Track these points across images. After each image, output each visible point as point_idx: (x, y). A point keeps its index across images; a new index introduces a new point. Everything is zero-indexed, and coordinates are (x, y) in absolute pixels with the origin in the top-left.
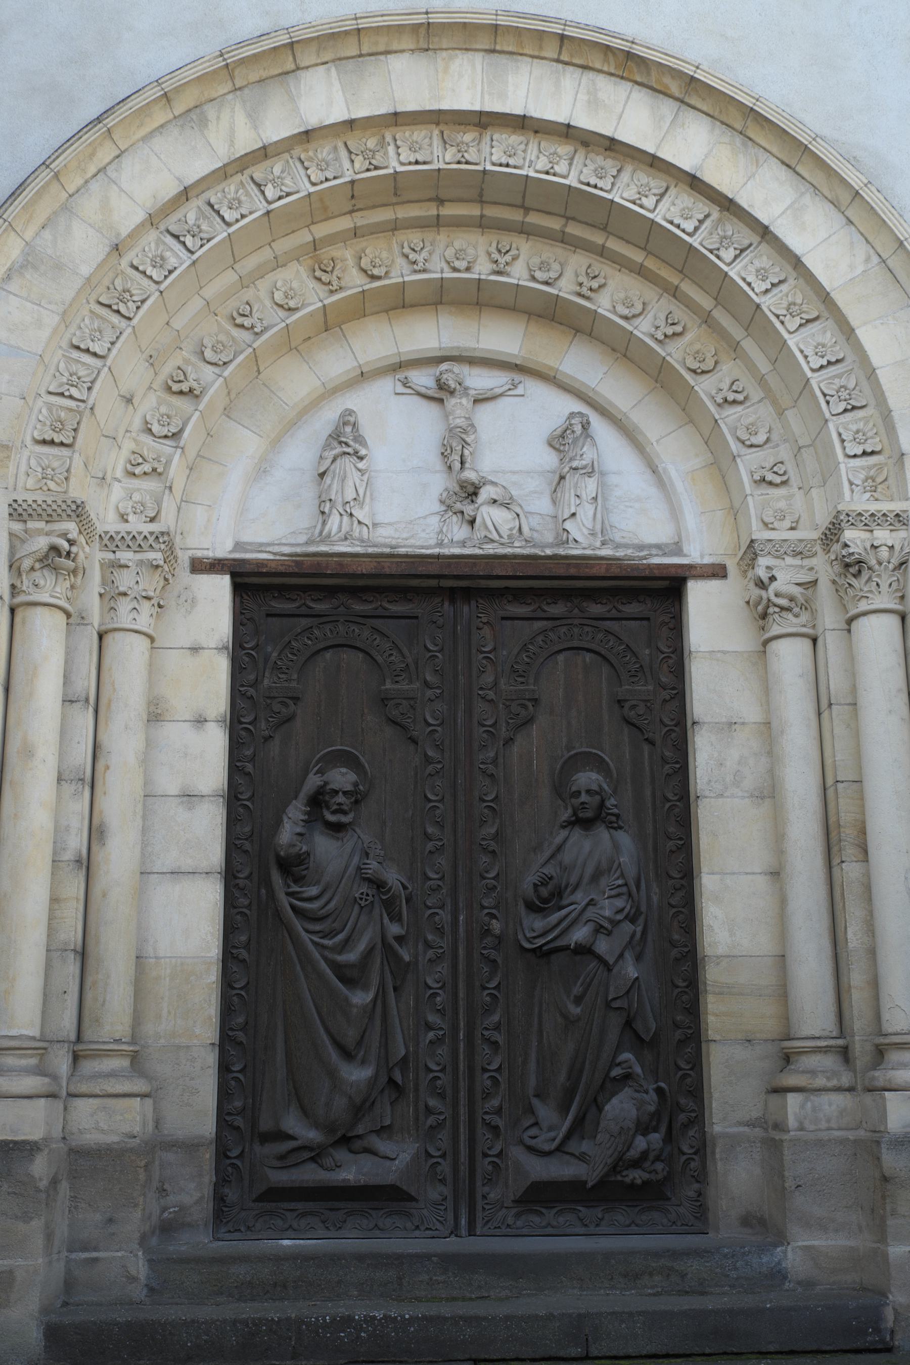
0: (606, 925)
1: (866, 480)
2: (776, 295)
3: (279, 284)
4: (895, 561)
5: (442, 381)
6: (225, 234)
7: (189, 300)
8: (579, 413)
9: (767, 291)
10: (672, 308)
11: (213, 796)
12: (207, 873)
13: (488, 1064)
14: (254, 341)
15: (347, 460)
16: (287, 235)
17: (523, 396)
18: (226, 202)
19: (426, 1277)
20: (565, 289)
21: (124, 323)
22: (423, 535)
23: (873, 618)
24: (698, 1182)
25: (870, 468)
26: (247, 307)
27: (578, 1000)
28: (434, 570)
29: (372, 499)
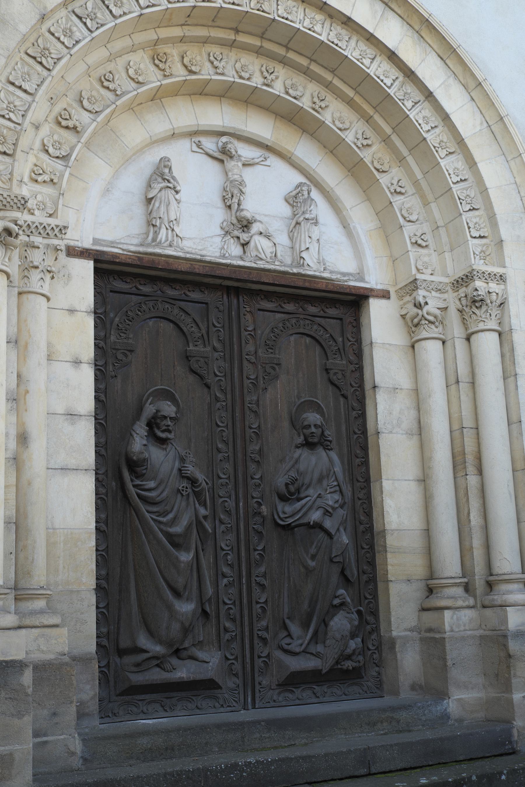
0: (330, 510)
1: (480, 253)
2: (433, 134)
4: (499, 302)
5: (227, 148)
9: (429, 131)
10: (365, 128)
11: (88, 416)
12: (86, 470)
13: (259, 599)
17: (269, 166)
19: (258, 735)
21: (45, 73)
22: (211, 249)
23: (487, 333)
24: (377, 666)
25: (484, 245)
26: (111, 75)
27: (313, 557)
28: (225, 273)
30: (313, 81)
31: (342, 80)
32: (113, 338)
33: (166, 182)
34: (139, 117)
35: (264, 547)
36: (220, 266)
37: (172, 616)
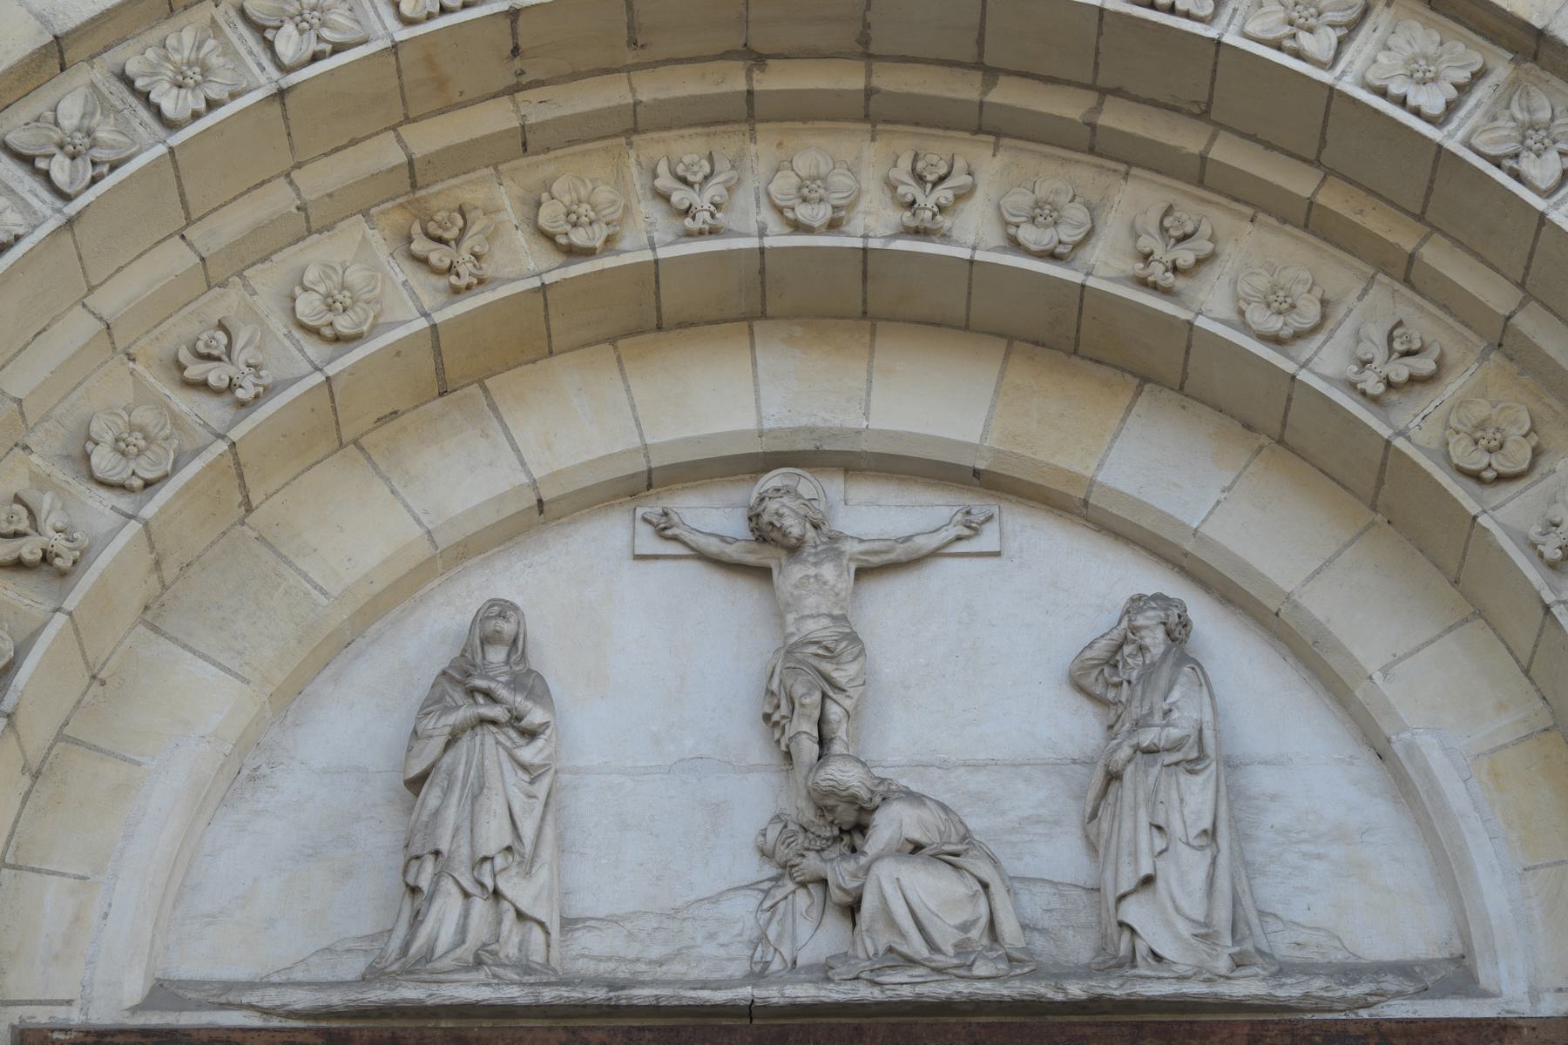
3: (311, 276)
5: (766, 518)
6: (161, 149)
7: (55, 319)
8: (1158, 597)
10: (1404, 311)
14: (234, 424)
15: (490, 741)
16: (337, 150)
17: (997, 554)
18: (168, 71)
20: (1105, 269)
22: (710, 949)
29: (561, 848)
30: (1134, 171)
31: (1253, 138)
33: (481, 699)
34: (382, 467)
36: (714, 1021)
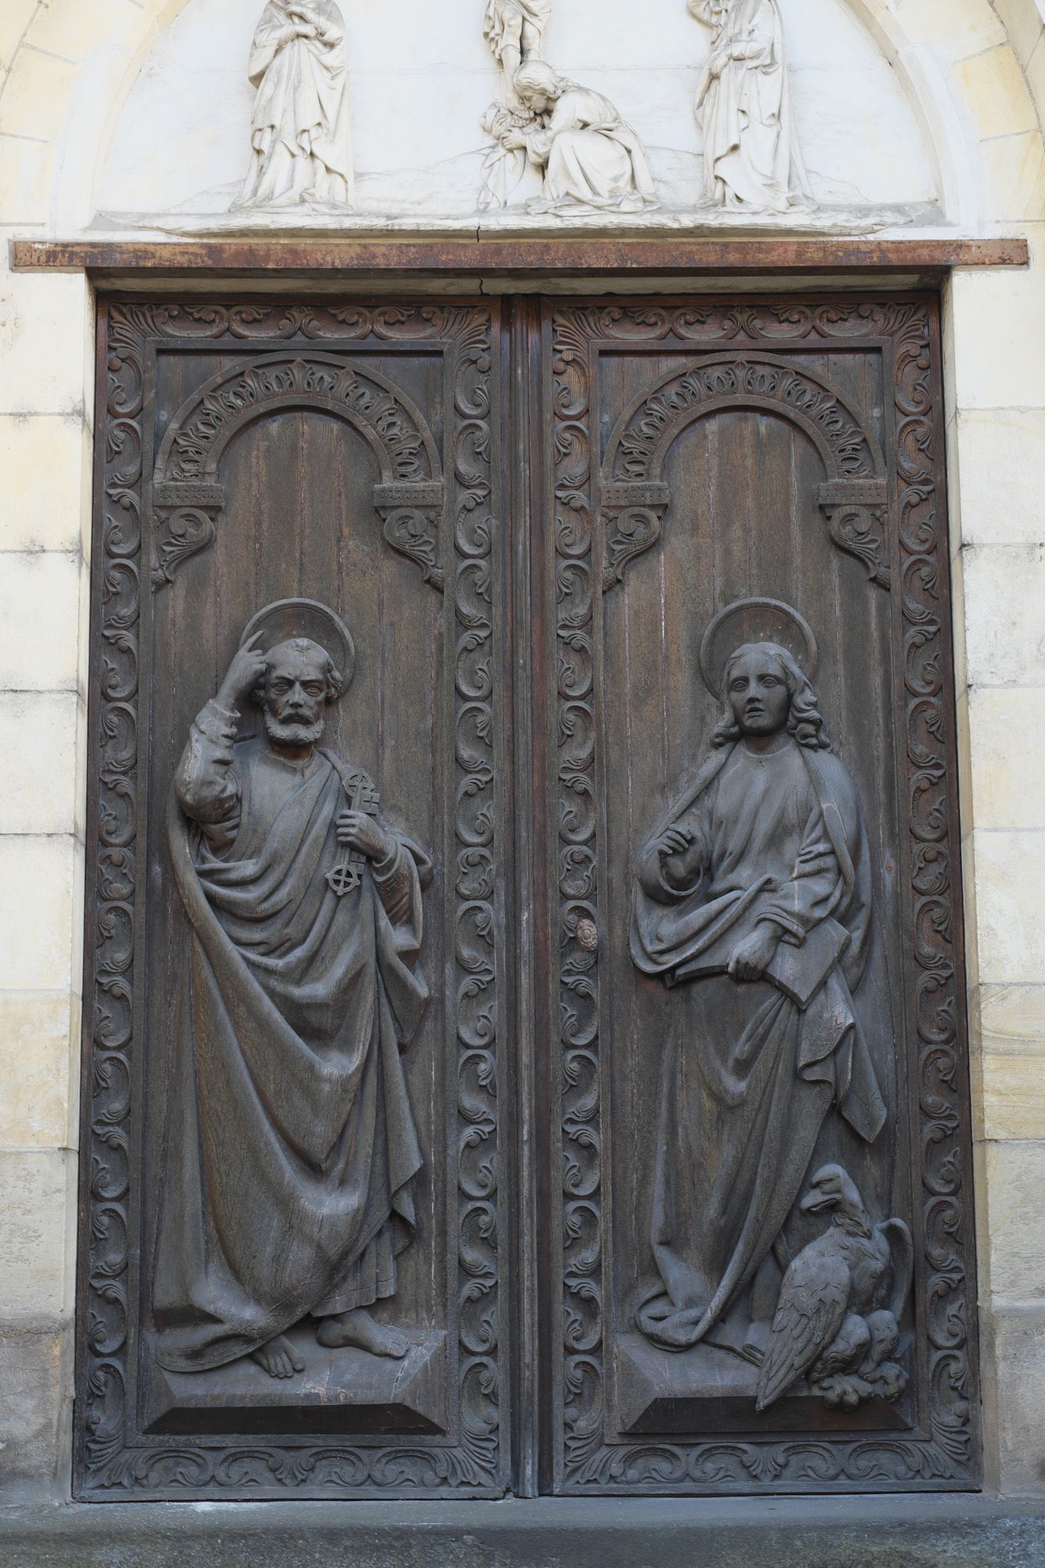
0: (795, 927)
11: (59, 692)
12: (49, 835)
13: (576, 1186)
27: (742, 1068)
32: (158, 477)
33: (296, 19)
35: (596, 1037)
36: (455, 241)
37: (291, 1227)
